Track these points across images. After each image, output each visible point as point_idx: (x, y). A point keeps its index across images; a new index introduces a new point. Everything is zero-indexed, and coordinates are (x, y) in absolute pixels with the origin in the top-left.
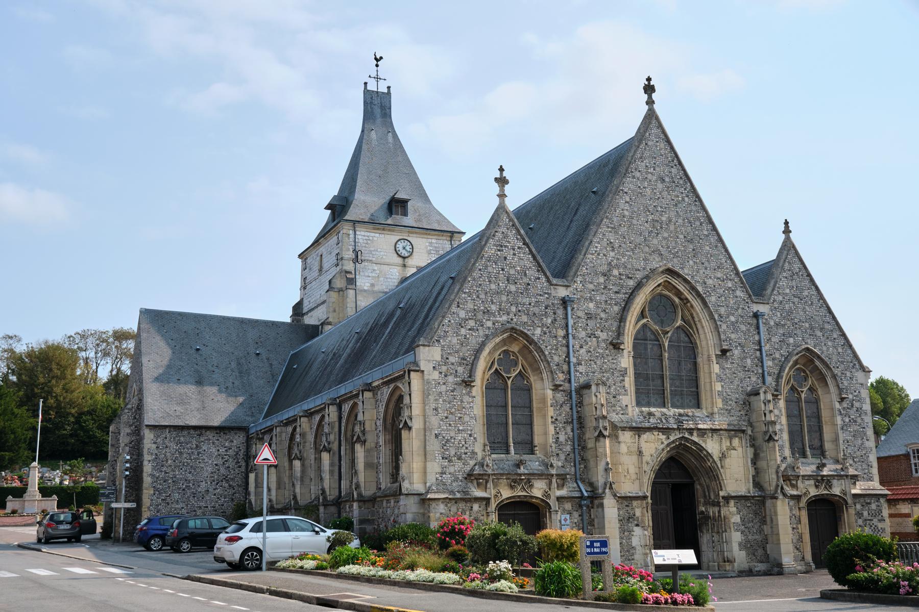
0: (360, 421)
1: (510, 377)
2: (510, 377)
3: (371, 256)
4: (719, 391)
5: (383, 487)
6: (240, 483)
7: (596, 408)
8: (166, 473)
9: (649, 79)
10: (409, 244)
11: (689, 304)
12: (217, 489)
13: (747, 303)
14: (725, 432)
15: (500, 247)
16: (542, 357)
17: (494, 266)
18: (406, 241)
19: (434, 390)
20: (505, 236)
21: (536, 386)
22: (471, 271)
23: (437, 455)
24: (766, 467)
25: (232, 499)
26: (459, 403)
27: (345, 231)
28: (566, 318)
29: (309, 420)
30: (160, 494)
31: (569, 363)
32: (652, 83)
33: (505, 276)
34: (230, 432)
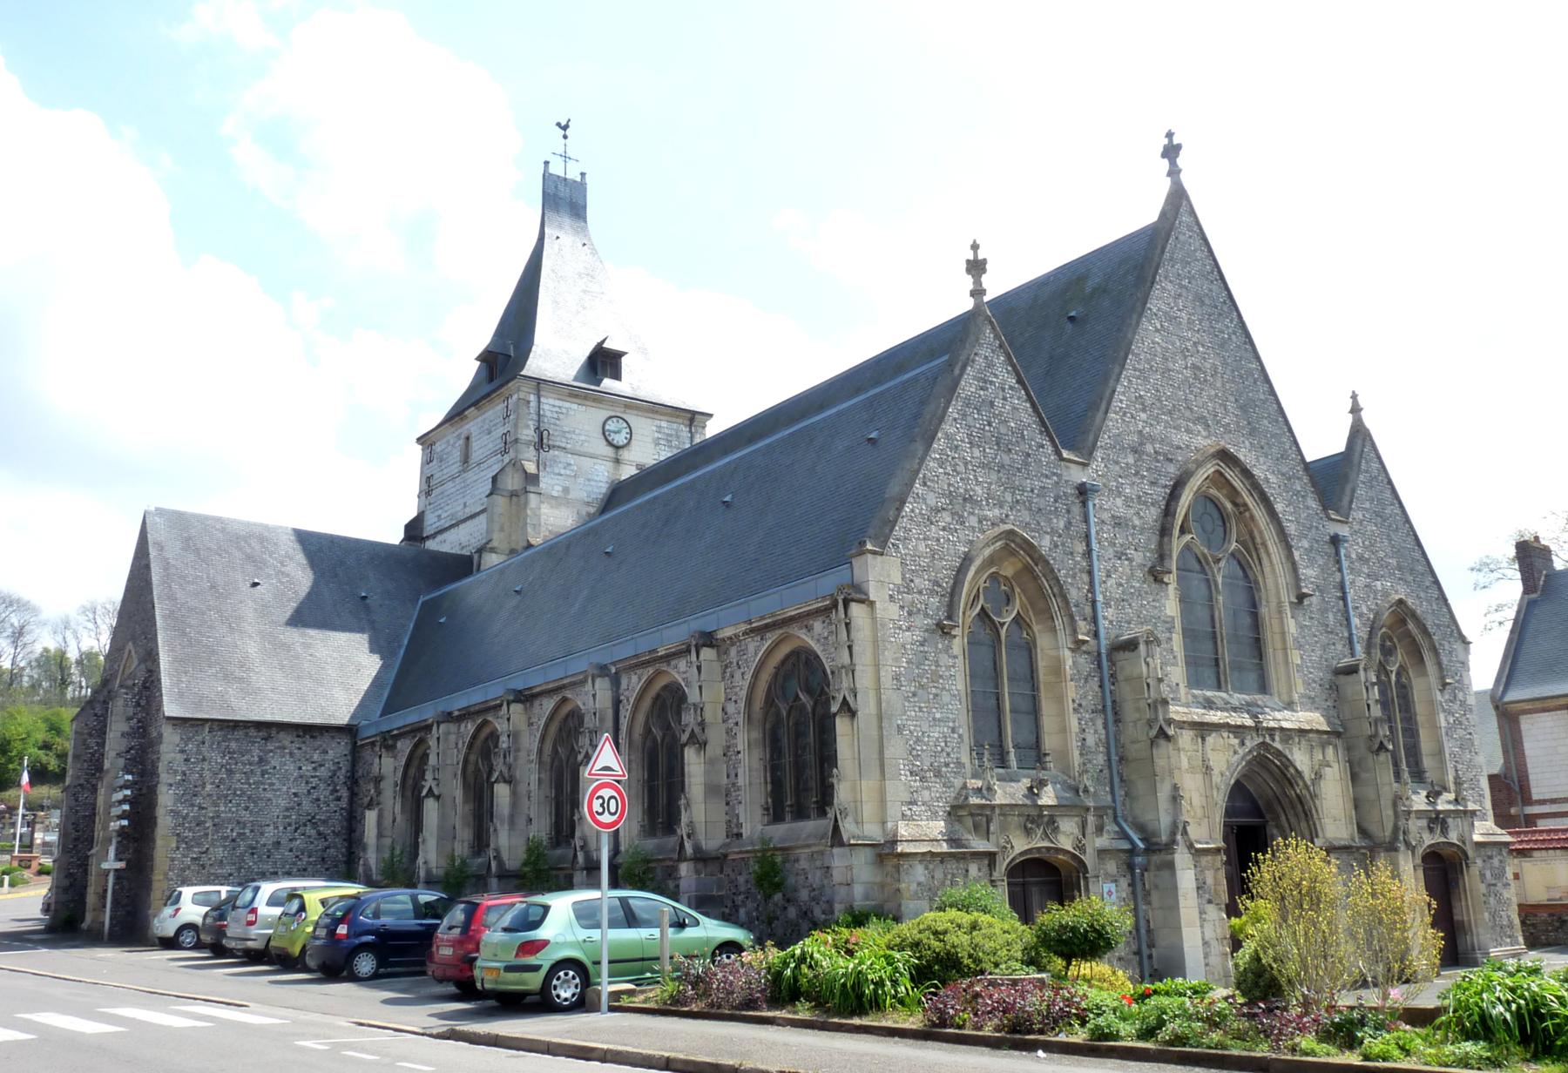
0: (694, 705)
1: (1004, 623)
2: (1004, 623)
3: (564, 440)
4: (1298, 665)
5: (746, 831)
6: (338, 829)
7: (1148, 685)
8: (201, 808)
9: (1170, 135)
10: (625, 425)
11: (1247, 514)
12: (295, 839)
13: (1321, 518)
14: (1315, 735)
15: (984, 382)
16: (1055, 590)
17: (976, 416)
18: (621, 421)
19: (893, 639)
20: (990, 365)
21: (1043, 642)
22: (941, 420)
23: (902, 767)
24: (1372, 796)
25: (323, 859)
26: (933, 668)
27: (522, 395)
28: (1086, 520)
29: (526, 709)
30: (189, 848)
31: (1094, 602)
32: (1176, 141)
33: (993, 436)
34: (322, 734)
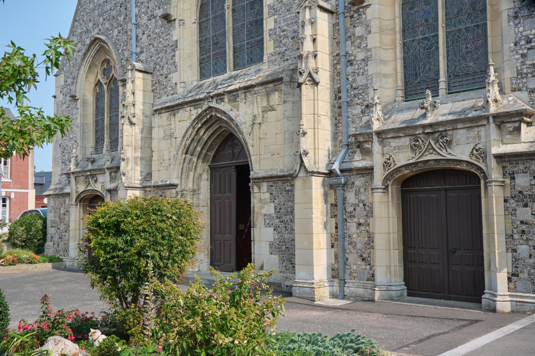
14: (260, 88)
